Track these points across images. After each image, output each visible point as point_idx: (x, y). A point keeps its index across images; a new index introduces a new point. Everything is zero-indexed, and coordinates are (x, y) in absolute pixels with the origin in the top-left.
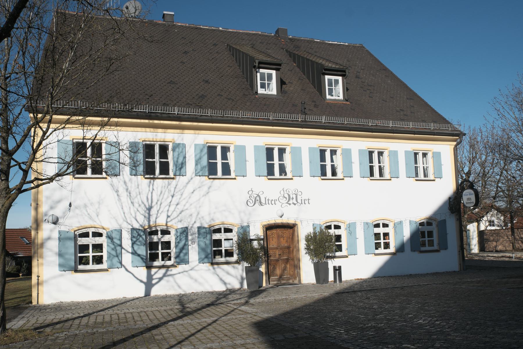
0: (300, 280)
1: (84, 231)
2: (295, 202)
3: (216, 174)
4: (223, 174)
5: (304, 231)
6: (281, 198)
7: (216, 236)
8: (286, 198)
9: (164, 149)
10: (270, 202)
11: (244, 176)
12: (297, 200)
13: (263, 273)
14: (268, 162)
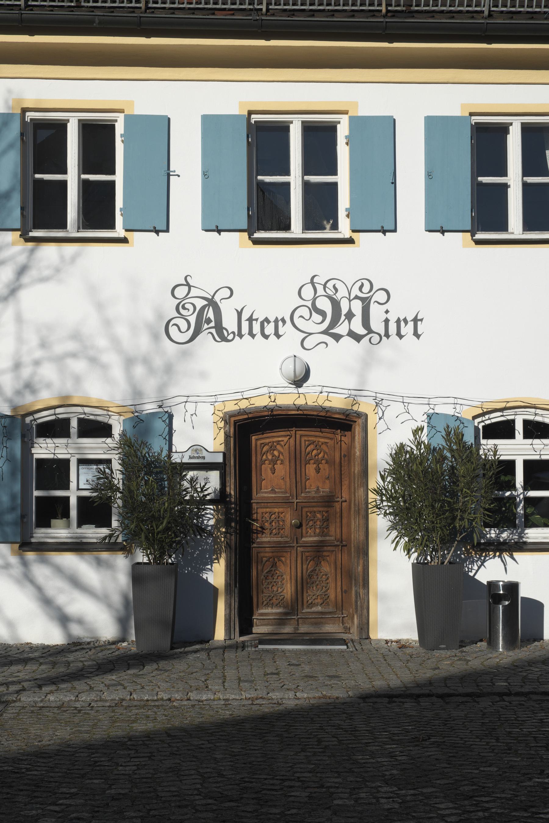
0: (365, 627)
1: (496, 418)
2: (361, 331)
3: (503, 226)
4: (310, 223)
5: (387, 438)
6: (305, 312)
7: (45, 449)
8: (323, 313)
9: (320, 139)
10: (267, 328)
11: (384, 232)
12: (366, 322)
13: (215, 590)
14: (84, 176)
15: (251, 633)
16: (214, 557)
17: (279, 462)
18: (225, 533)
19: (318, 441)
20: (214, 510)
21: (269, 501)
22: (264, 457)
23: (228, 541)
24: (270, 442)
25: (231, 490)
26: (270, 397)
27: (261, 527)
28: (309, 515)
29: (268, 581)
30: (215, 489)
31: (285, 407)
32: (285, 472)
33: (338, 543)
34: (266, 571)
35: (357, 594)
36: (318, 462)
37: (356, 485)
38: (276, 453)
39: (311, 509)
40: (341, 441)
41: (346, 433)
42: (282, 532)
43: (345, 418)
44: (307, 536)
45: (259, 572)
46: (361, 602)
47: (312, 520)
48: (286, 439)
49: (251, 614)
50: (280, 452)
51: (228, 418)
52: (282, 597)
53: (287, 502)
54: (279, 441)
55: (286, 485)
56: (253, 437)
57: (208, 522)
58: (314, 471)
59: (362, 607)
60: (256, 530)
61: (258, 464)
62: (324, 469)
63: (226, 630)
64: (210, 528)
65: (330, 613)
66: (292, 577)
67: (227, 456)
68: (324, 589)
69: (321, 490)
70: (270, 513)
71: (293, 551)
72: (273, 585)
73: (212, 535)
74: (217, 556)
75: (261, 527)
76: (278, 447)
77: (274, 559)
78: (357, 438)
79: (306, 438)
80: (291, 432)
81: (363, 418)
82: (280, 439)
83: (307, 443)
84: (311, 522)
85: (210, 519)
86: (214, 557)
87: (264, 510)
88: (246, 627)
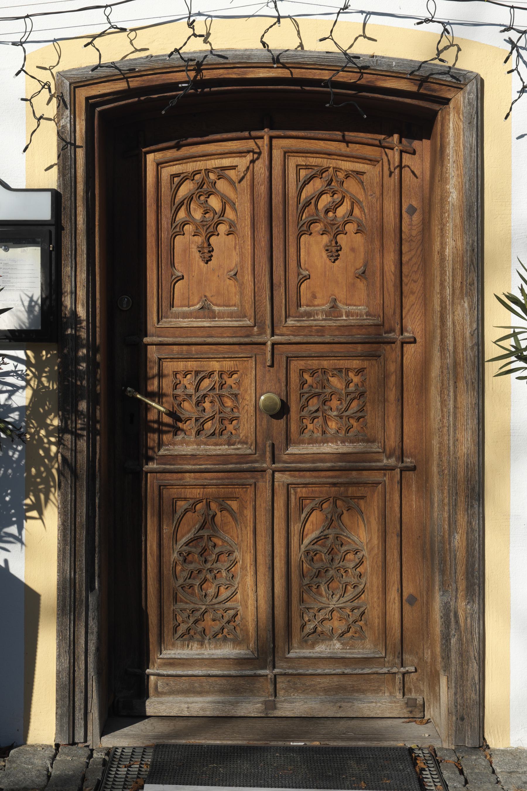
0: (470, 713)
13: (32, 598)
15: (142, 716)
16: (28, 501)
17: (222, 228)
18: (61, 431)
19: (337, 169)
20: (27, 363)
21: (194, 340)
22: (182, 214)
23: (68, 454)
24: (198, 172)
25: (77, 302)
26: (191, 25)
27: (171, 414)
28: (309, 380)
29: (191, 567)
30: (31, 300)
31: (236, 56)
32: (242, 255)
33: (392, 461)
34: (184, 540)
35: (449, 616)
36: (335, 230)
37: (448, 291)
38: (215, 203)
39: (314, 364)
40: (401, 167)
41: (416, 144)
42: (230, 427)
43: (414, 89)
44: (301, 442)
45: (165, 541)
46: (460, 640)
47: (318, 395)
48: (243, 162)
49: (143, 659)
50: (225, 201)
51: (69, 90)
52: (232, 612)
53: (245, 344)
54: (224, 168)
55: (242, 294)
56: (150, 157)
57: (9, 398)
58: (324, 254)
59: (462, 654)
60: (158, 422)
61: (164, 235)
62: (353, 250)
63: (59, 717)
64: (15, 416)
65: (366, 661)
66: (260, 558)
67: (66, 202)
68: (351, 593)
69: (344, 308)
70: (197, 373)
71: (260, 484)
72: (205, 580)
73: (21, 436)
74: (38, 498)
75: (171, 414)
76: (222, 185)
77: (208, 505)
78: (450, 150)
79: (301, 161)
80: (259, 142)
81: (471, 87)
82: (226, 162)
83: (303, 173)
84: (315, 400)
85: (16, 389)
86: (28, 501)
87: (181, 366)
88: (123, 700)
